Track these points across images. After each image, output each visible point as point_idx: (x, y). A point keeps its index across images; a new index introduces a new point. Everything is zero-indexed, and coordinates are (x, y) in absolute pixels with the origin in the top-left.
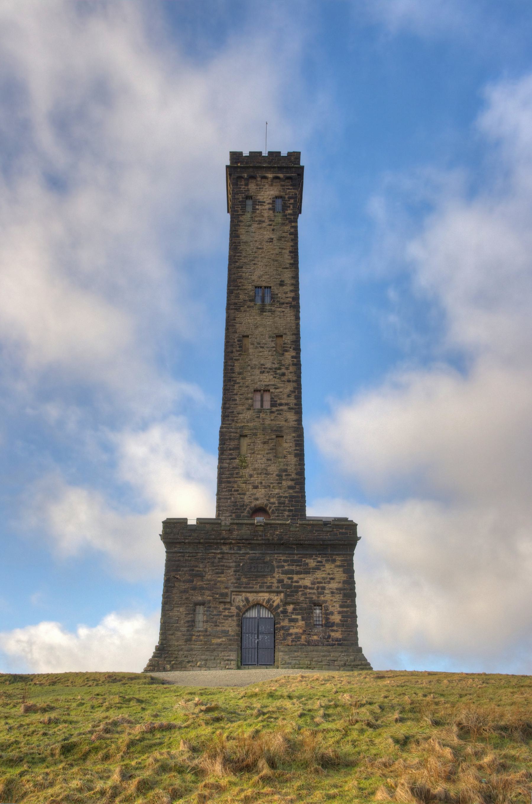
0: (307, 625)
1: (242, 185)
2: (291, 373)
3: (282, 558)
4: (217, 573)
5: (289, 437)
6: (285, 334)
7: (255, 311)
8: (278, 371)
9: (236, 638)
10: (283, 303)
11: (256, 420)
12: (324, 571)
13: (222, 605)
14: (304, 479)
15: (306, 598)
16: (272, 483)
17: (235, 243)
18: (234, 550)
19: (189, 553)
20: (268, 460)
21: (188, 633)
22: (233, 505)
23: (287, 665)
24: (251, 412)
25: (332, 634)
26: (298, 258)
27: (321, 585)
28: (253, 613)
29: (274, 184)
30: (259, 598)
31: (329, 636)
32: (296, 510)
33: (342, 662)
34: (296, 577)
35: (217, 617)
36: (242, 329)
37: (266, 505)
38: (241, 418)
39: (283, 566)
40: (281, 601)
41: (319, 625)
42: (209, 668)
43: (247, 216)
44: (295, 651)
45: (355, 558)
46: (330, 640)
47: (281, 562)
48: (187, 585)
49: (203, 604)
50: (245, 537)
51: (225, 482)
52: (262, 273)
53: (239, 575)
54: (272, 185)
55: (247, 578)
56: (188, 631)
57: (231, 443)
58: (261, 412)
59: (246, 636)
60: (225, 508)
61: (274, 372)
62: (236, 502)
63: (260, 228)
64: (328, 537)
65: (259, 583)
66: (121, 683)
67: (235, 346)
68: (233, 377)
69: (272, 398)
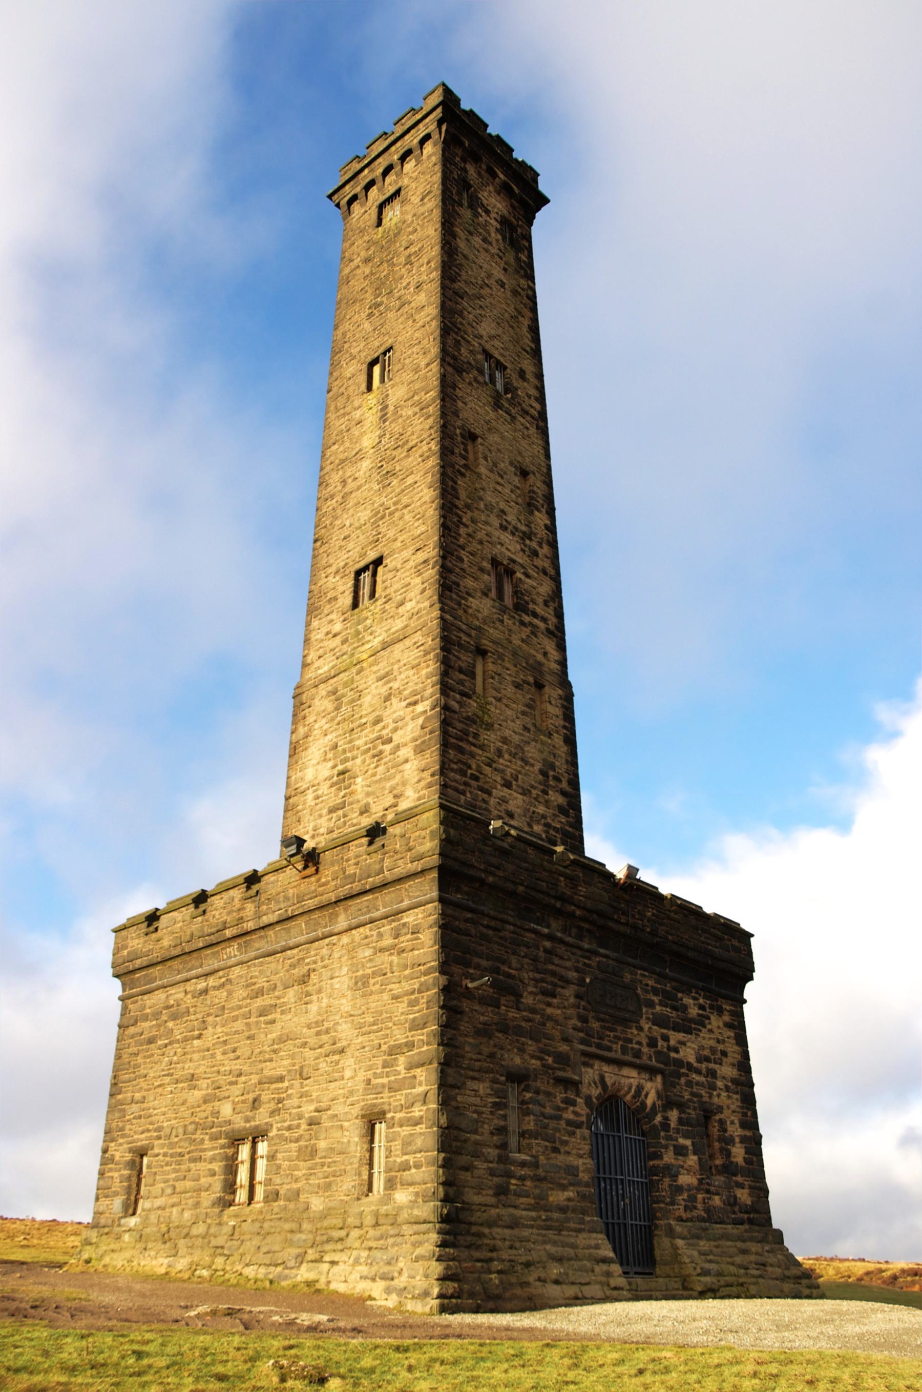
34: (675, 1037)
45: (748, 1010)
46: (737, 1209)
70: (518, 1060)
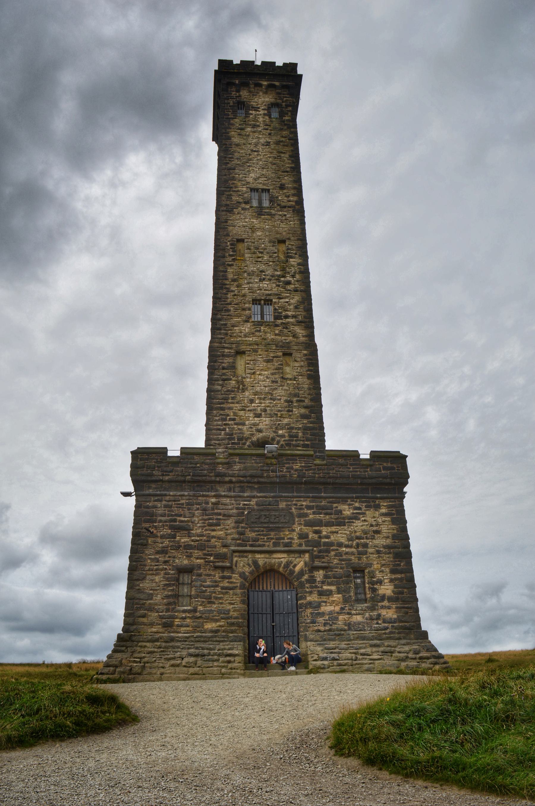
0: (346, 600)
1: (233, 91)
4: (211, 525)
6: (289, 239)
8: (282, 279)
10: (285, 207)
15: (341, 560)
16: (279, 411)
18: (234, 492)
20: (273, 382)
22: (228, 438)
24: (249, 325)
25: (383, 612)
30: (273, 561)
34: (325, 531)
38: (237, 331)
40: (306, 564)
44: (330, 640)
45: (407, 502)
51: (217, 409)
52: (258, 175)
54: (266, 93)
55: (254, 531)
60: (217, 442)
61: (277, 279)
63: (254, 132)
65: (272, 539)
70: (186, 562)
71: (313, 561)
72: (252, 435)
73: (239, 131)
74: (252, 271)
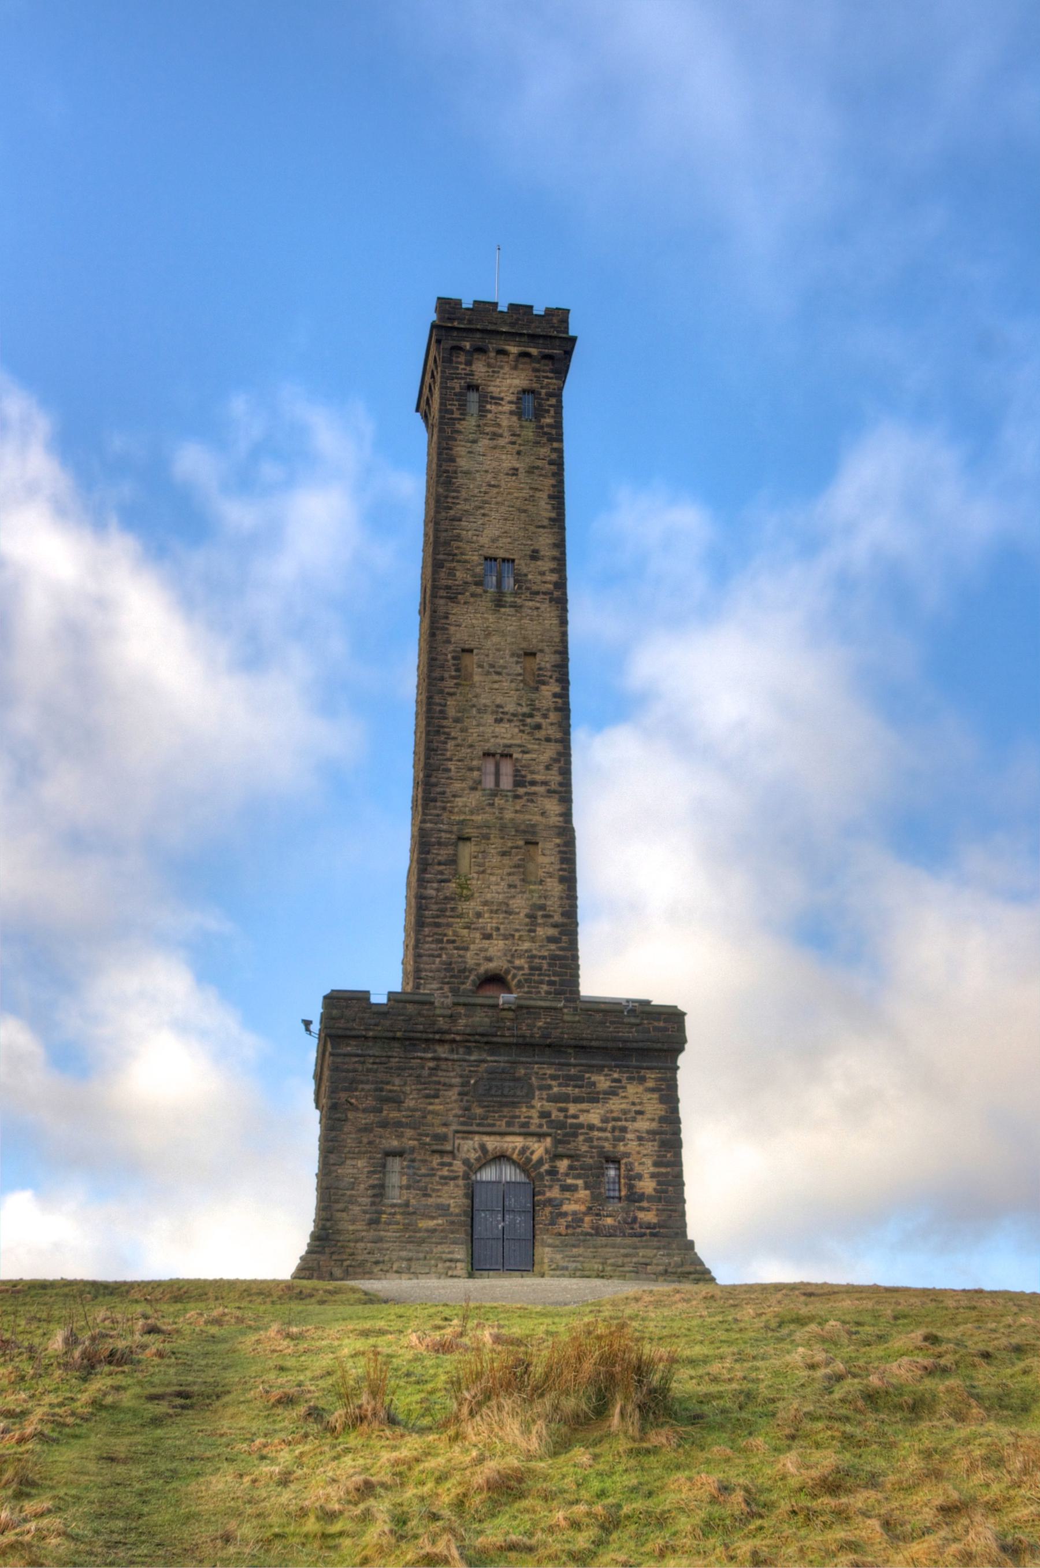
0: (595, 1198)
1: (460, 363)
2: (552, 724)
3: (548, 1072)
4: (427, 1097)
5: (550, 845)
6: (541, 651)
7: (485, 603)
8: (529, 720)
9: (463, 1218)
10: (538, 593)
11: (487, 809)
12: (625, 1097)
13: (437, 1156)
14: (576, 924)
15: (591, 1147)
16: (517, 930)
17: (447, 471)
19: (374, 1056)
20: (510, 886)
21: (374, 1208)
23: (560, 1271)
25: (641, 1215)
26: (564, 509)
27: (619, 1123)
28: (488, 1174)
29: (521, 366)
30: (506, 1145)
31: (635, 1219)
32: (562, 983)
33: (661, 1268)
34: (573, 1109)
35: (428, 1179)
36: (460, 635)
37: (507, 972)
38: (460, 804)
39: (550, 1087)
40: (547, 1151)
41: (613, 1198)
42: (416, 1275)
43: (470, 423)
44: (574, 1246)
45: (681, 1076)
46: (637, 1226)
47: (545, 1079)
48: (371, 1118)
49: (399, 1154)
50: (480, 1030)
51: (430, 925)
52: (497, 533)
53: (467, 1101)
54: (515, 368)
56: (373, 1204)
57: (442, 852)
58: (496, 795)
59: (481, 1216)
60: (430, 974)
61: (521, 721)
62: (450, 964)
64: (632, 1034)
65: (505, 1117)
66: (313, 1300)
67: (443, 670)
68: (443, 727)
69: (517, 770)
71: (556, 1147)
72: (479, 965)
73: (469, 444)
74: (485, 706)
